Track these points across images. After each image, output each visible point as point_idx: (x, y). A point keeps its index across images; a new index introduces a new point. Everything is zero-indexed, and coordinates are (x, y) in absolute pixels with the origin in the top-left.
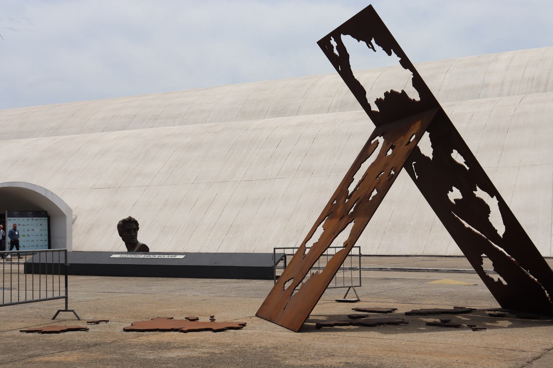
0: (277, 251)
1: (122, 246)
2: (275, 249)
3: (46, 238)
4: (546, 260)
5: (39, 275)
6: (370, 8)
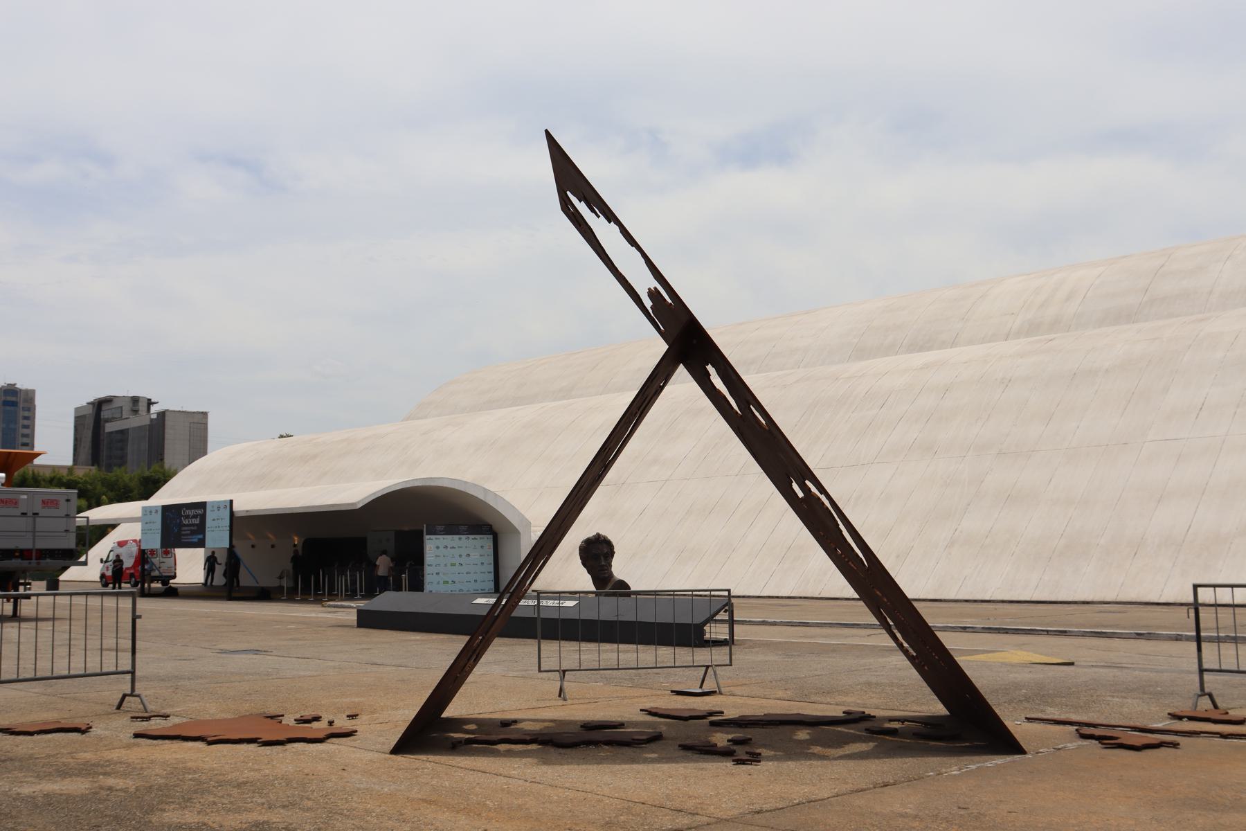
0: (1205, 596)
1: (584, 581)
2: (1196, 587)
3: (491, 568)
4: (915, 604)
5: (534, 642)
6: (205, 414)
